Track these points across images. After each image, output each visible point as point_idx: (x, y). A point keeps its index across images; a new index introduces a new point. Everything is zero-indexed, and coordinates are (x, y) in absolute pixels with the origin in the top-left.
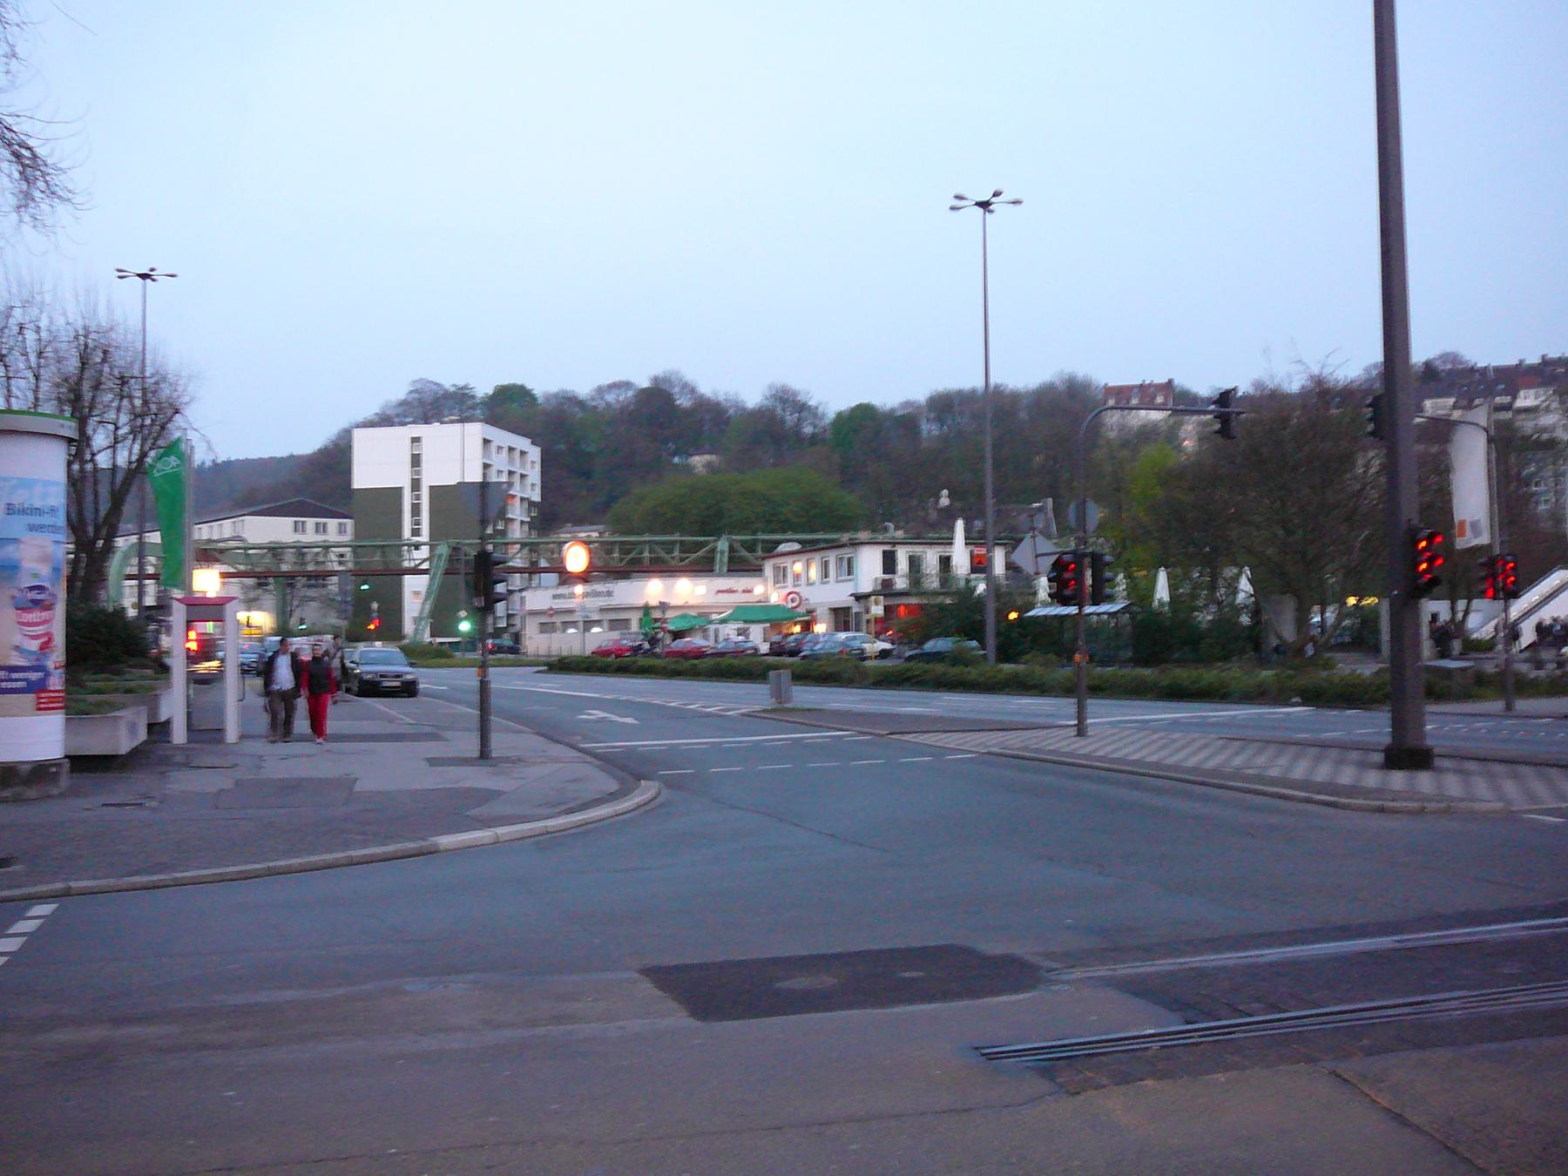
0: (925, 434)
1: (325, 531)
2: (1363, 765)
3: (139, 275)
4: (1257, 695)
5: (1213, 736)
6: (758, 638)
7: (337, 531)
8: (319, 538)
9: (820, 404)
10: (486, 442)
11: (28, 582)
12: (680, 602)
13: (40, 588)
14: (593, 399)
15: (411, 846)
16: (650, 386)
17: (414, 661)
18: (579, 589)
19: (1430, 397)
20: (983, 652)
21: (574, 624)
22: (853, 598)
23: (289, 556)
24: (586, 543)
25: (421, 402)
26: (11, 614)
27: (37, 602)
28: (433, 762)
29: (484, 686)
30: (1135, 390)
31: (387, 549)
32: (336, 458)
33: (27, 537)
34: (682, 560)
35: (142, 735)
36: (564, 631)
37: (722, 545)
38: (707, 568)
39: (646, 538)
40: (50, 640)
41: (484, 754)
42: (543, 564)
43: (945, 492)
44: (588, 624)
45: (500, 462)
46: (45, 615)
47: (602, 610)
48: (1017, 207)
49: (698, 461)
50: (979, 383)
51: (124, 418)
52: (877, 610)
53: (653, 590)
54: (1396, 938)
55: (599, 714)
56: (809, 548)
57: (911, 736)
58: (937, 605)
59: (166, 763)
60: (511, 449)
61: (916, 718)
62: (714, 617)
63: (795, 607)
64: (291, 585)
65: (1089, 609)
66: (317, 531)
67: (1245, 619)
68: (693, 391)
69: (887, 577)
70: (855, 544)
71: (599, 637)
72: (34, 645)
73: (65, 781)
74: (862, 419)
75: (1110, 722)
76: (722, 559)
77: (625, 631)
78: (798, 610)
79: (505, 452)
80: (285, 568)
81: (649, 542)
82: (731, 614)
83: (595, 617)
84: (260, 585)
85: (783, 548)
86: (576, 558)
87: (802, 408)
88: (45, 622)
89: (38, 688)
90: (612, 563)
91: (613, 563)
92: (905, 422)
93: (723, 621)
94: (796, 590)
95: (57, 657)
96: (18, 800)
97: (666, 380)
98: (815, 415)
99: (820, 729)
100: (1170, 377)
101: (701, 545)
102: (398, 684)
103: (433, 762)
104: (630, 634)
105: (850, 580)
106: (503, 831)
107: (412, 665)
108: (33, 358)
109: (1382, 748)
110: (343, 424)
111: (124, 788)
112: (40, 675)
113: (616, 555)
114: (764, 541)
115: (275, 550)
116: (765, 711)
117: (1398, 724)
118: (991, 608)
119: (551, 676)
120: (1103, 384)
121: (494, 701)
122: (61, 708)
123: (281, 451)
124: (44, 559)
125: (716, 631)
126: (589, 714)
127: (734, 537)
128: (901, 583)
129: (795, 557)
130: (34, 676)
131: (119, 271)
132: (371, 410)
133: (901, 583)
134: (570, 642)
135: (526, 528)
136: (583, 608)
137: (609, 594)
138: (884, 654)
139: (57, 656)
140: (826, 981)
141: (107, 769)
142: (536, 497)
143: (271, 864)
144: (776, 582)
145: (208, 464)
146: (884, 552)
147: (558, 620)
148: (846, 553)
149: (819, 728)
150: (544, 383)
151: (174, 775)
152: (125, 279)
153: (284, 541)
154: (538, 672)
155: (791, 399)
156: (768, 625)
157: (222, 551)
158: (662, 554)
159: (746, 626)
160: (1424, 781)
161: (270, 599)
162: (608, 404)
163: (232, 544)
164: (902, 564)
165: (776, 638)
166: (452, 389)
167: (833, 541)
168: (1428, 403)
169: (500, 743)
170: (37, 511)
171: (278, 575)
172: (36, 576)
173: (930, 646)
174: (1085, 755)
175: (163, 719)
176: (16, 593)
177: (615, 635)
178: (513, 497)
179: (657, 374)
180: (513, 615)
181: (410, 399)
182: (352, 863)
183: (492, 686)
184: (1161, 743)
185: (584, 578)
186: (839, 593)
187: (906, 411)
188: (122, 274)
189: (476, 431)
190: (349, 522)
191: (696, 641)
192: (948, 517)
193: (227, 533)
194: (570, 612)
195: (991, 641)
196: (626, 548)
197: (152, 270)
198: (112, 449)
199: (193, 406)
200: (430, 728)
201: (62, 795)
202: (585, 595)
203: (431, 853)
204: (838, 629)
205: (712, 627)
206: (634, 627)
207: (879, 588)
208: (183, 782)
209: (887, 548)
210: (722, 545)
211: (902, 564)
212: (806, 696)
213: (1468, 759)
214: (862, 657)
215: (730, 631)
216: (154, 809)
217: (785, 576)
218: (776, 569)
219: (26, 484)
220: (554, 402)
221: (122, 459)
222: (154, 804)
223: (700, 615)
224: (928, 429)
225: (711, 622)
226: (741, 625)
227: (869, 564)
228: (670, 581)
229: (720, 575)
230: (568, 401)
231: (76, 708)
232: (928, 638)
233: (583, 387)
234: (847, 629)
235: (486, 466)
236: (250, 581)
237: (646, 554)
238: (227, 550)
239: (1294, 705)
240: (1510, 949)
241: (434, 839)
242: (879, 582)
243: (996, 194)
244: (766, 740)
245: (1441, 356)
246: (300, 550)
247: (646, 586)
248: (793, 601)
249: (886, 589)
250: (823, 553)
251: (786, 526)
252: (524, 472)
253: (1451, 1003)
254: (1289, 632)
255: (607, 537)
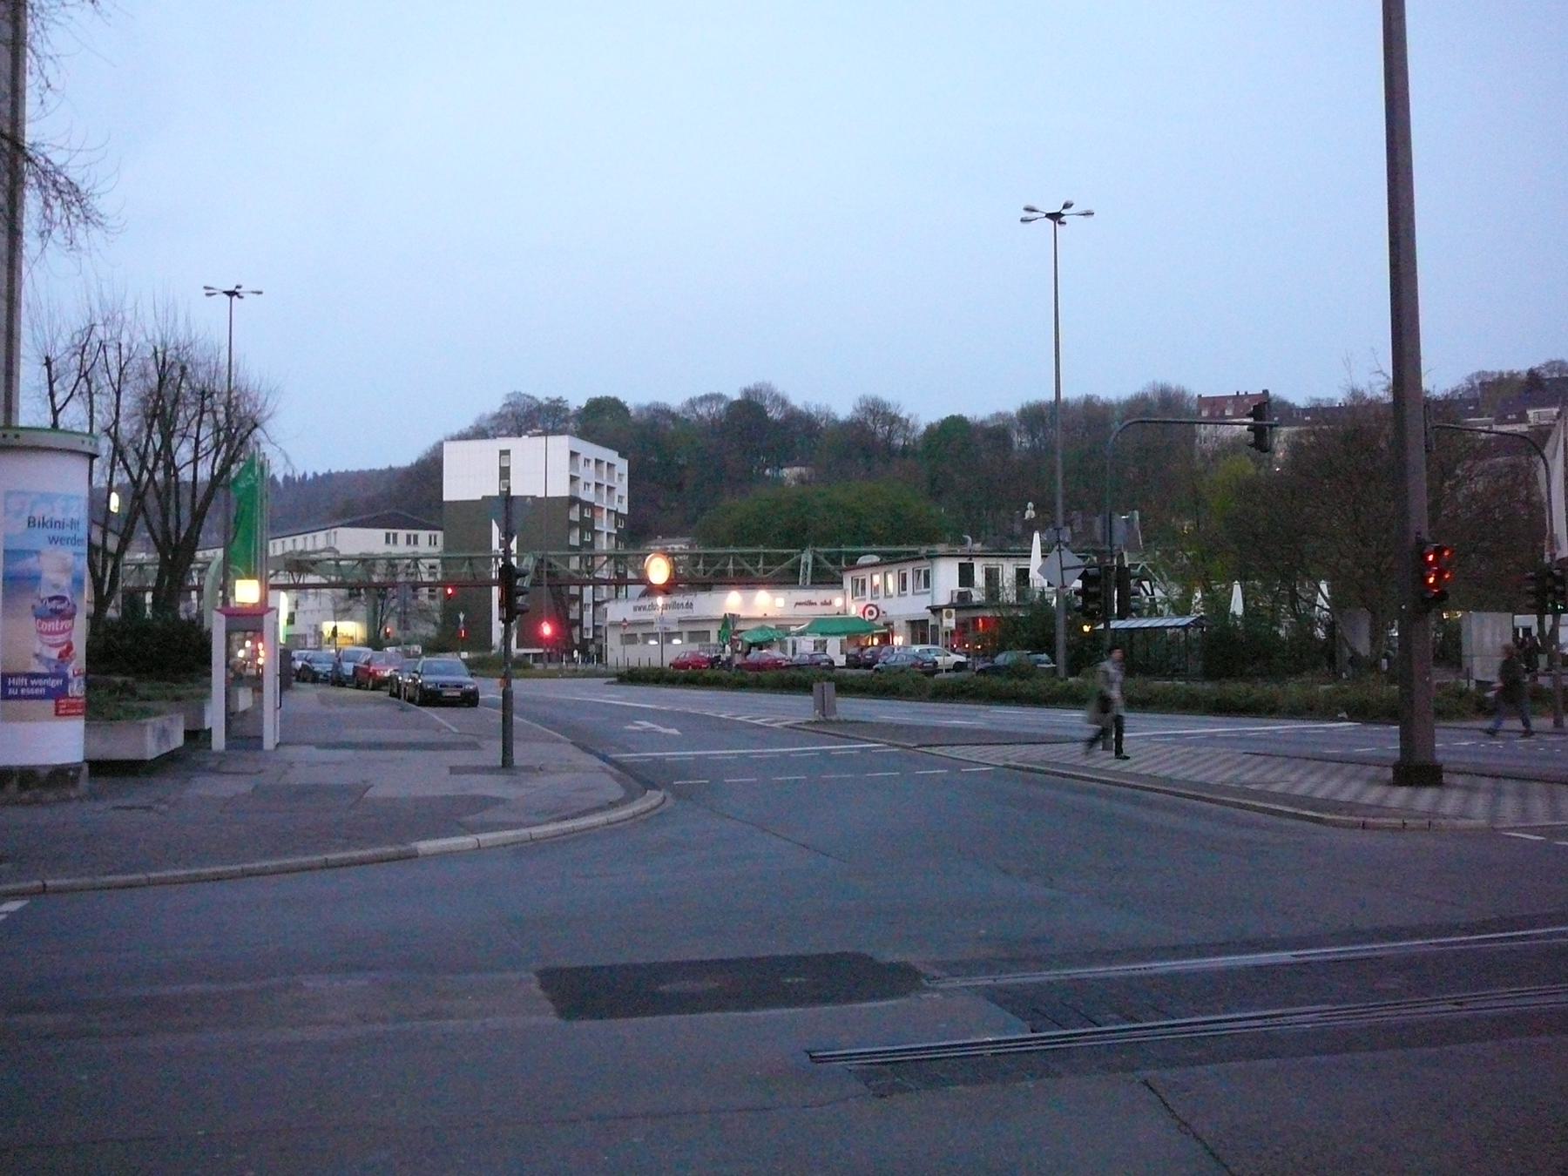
0: (1016, 447)
1: (416, 542)
2: (1373, 781)
3: (225, 292)
4: (1295, 713)
5: (1238, 751)
6: (835, 652)
7: (428, 543)
8: (410, 550)
9: (910, 416)
10: (573, 455)
11: (46, 592)
12: (760, 615)
13: (62, 599)
14: (684, 412)
15: (390, 850)
16: (1424, 389)
17: (474, 671)
18: (660, 601)
19: (1535, 406)
20: (1052, 665)
21: (655, 636)
22: (929, 611)
23: (381, 567)
24: (670, 555)
25: (515, 416)
26: (32, 623)
27: (59, 611)
28: (454, 770)
29: (507, 696)
30: (1230, 402)
31: (474, 561)
32: (429, 471)
33: (47, 549)
34: (766, 572)
35: (178, 740)
36: (646, 642)
37: (807, 557)
38: (793, 580)
39: (732, 550)
40: (70, 648)
41: (507, 763)
42: (631, 575)
43: (1030, 505)
44: (669, 636)
45: (587, 474)
46: (66, 624)
47: (681, 622)
48: (1090, 218)
49: (789, 473)
50: (1048, 395)
51: (206, 431)
52: (950, 623)
53: (733, 601)
54: (1295, 953)
55: (647, 724)
56: (889, 560)
57: (937, 749)
58: (1010, 618)
59: (201, 769)
60: (598, 462)
61: (958, 731)
62: (793, 629)
63: (875, 619)
64: (383, 597)
65: (1114, 624)
66: (408, 542)
67: (1320, 633)
68: (784, 403)
69: (963, 589)
70: (932, 557)
71: (679, 648)
72: (54, 653)
73: (84, 782)
74: (954, 431)
75: (1142, 737)
76: (806, 572)
77: (704, 643)
78: (876, 622)
79: (593, 463)
80: (375, 579)
81: (733, 553)
82: (809, 626)
83: (675, 629)
84: (351, 596)
85: (862, 560)
86: (658, 570)
87: (893, 420)
88: (64, 631)
89: (58, 694)
90: (698, 575)
91: (700, 575)
92: (995, 434)
93: (801, 633)
94: (874, 602)
95: (78, 662)
96: (37, 801)
97: (756, 392)
98: (906, 428)
99: (852, 741)
100: (1265, 388)
101: (787, 557)
102: (458, 694)
103: (454, 770)
104: (709, 645)
105: (928, 592)
106: (487, 838)
107: (472, 675)
108: (115, 375)
109: (1392, 764)
110: (441, 437)
111: (138, 793)
112: (59, 682)
113: (700, 567)
114: (847, 554)
115: (367, 561)
116: (809, 723)
117: (1406, 738)
118: (1061, 623)
119: (621, 687)
120: (1196, 396)
121: (516, 705)
122: (79, 714)
123: (381, 464)
124: (66, 570)
125: (794, 643)
126: (638, 725)
127: (818, 550)
128: (977, 596)
129: (874, 569)
130: (54, 683)
131: (206, 288)
132: (466, 423)
133: (977, 596)
134: (649, 654)
135: (613, 540)
136: (662, 620)
137: (690, 606)
138: (959, 667)
139: (78, 662)
140: (709, 984)
141: (135, 774)
142: (624, 509)
143: (246, 866)
144: (855, 594)
145: (310, 476)
146: (960, 564)
147: (639, 631)
148: (923, 565)
149: (847, 739)
150: (636, 397)
151: (199, 780)
152: (214, 297)
153: (376, 552)
154: (608, 683)
155: (881, 411)
156: (845, 638)
157: (314, 563)
158: (747, 567)
159: (823, 638)
160: (1425, 797)
161: (362, 610)
162: (700, 417)
163: (325, 555)
164: (979, 578)
165: (853, 650)
166: (545, 402)
167: (915, 553)
168: (1531, 413)
169: (520, 754)
170: (60, 525)
171: (369, 586)
172: (56, 586)
173: (1001, 659)
174: (1115, 771)
175: (207, 727)
176: (38, 604)
177: (695, 647)
178: (602, 509)
179: (747, 386)
180: (599, 627)
181: (503, 413)
182: (327, 866)
183: (480, 697)
184: (1225, 756)
185: (667, 589)
186: (915, 606)
187: (996, 423)
188: (210, 292)
189: (561, 445)
190: (440, 534)
191: (775, 653)
192: (1030, 527)
193: (321, 543)
194: (651, 623)
195: (1061, 655)
196: (710, 560)
197: (238, 287)
198: (192, 464)
199: (270, 421)
200: (471, 737)
201: (80, 799)
202: (666, 607)
203: (409, 857)
204: (914, 642)
205: (789, 639)
206: (714, 639)
207: (955, 601)
208: (207, 788)
209: (964, 560)
210: (807, 557)
211: (979, 578)
212: (851, 708)
213: (1505, 777)
214: (934, 669)
215: (806, 645)
216: (162, 813)
217: (863, 588)
218: (855, 581)
219: (48, 498)
220: (645, 415)
221: (204, 472)
222: (164, 807)
223: (778, 627)
224: (1021, 441)
225: (788, 635)
226: (819, 638)
227: (946, 576)
228: (749, 593)
229: (804, 587)
230: (660, 415)
231: (95, 712)
232: (1002, 649)
233: (675, 398)
234: (924, 641)
235: (573, 479)
236: (343, 592)
237: (731, 567)
238: (321, 561)
239: (1342, 720)
240: (1408, 964)
241: (414, 845)
242: (956, 595)
243: (1066, 206)
244: (793, 752)
245: (1547, 365)
246: (391, 562)
247: (754, 596)
248: (871, 613)
249: (962, 602)
250: (899, 566)
251: (871, 539)
252: (611, 485)
253: (1304, 1017)
254: (1363, 647)
255: (697, 550)
